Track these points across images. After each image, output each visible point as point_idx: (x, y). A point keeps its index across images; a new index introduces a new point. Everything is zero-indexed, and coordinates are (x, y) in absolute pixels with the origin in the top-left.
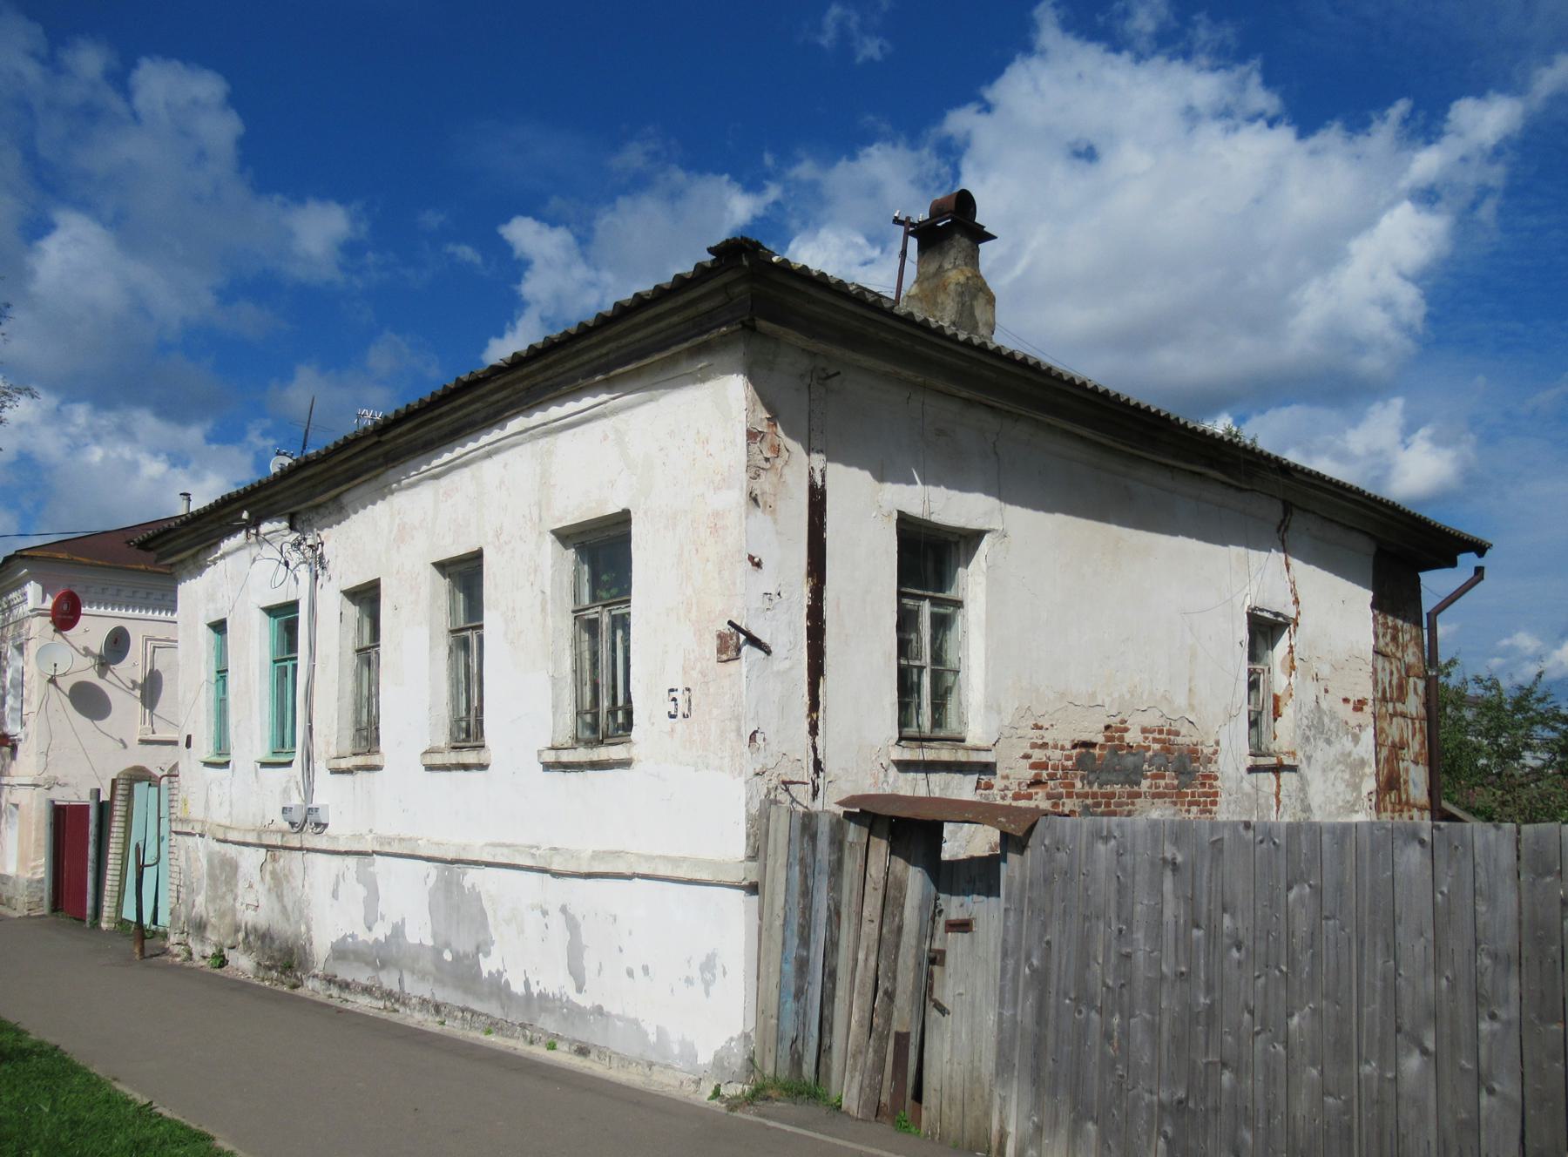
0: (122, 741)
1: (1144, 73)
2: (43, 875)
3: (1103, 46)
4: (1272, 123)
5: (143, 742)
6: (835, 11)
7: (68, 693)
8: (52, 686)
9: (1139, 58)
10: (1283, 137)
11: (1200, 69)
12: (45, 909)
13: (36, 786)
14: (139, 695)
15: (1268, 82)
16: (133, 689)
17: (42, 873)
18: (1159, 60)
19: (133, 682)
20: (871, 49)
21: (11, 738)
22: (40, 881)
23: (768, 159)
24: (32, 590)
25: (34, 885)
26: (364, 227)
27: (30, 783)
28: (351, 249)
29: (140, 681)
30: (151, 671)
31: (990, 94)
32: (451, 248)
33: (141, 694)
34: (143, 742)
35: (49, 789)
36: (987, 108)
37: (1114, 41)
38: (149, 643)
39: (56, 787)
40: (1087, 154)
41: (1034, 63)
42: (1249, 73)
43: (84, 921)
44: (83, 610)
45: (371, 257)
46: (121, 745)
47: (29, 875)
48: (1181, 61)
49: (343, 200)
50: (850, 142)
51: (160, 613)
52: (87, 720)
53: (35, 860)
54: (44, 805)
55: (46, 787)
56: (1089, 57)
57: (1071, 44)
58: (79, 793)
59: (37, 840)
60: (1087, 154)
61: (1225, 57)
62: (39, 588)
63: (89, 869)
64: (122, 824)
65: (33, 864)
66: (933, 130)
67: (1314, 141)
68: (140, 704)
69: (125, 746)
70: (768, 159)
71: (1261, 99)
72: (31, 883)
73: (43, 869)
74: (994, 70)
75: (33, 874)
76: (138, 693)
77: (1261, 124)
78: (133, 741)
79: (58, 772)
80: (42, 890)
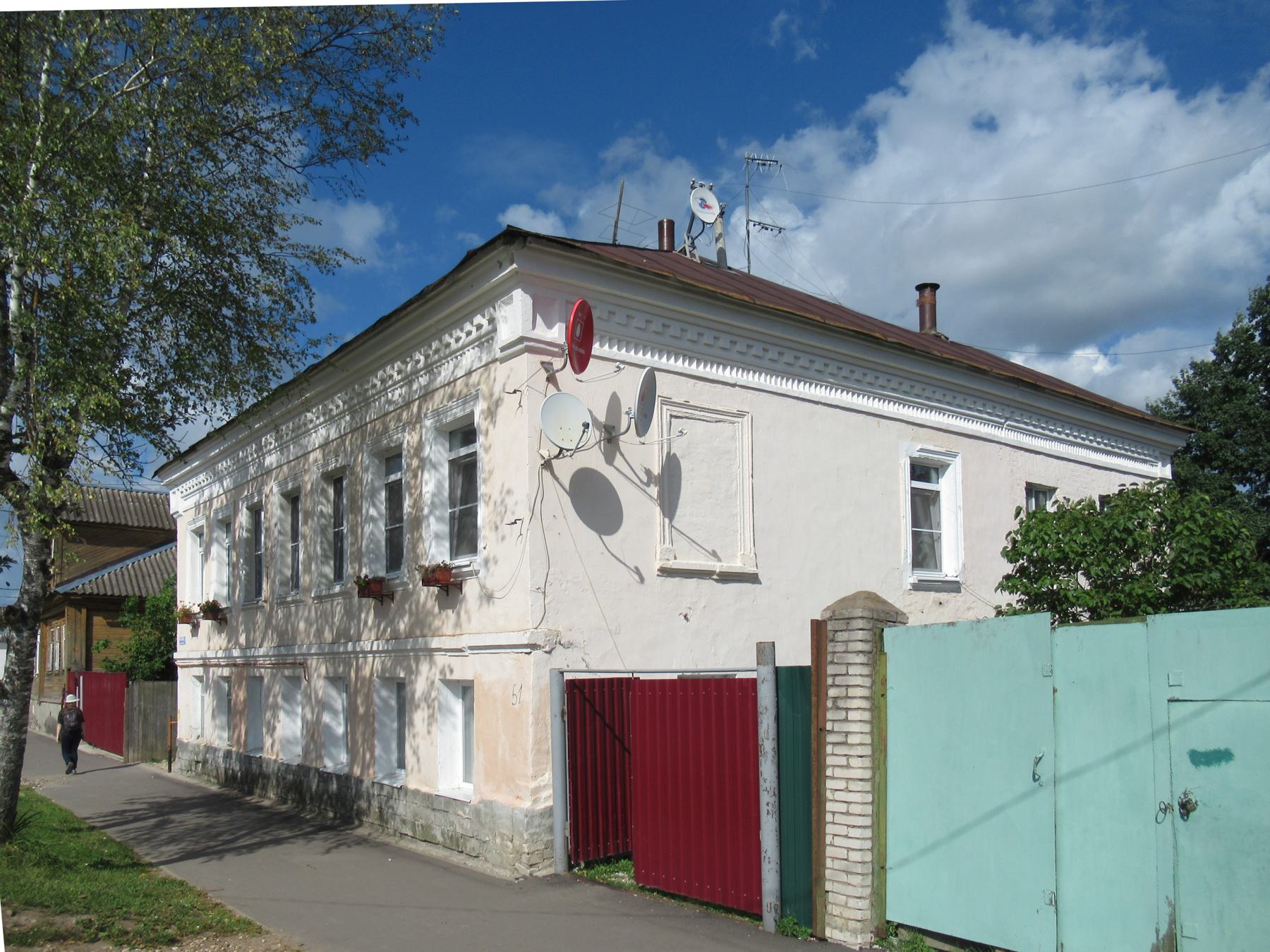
0: (637, 571)
1: (1042, 52)
2: (550, 803)
3: (1006, 31)
4: (1155, 87)
5: (666, 572)
6: (782, 17)
7: (567, 486)
8: (546, 474)
9: (1038, 38)
10: (1165, 97)
11: (1092, 46)
12: (556, 864)
13: (534, 647)
14: (655, 495)
15: (1153, 52)
16: (648, 484)
17: (547, 798)
18: (1058, 39)
19: (648, 472)
20: (806, 50)
21: (454, 571)
22: (549, 812)
23: (722, 143)
24: (518, 304)
25: (536, 822)
26: (394, 225)
27: (526, 642)
28: (384, 241)
29: (656, 470)
30: (668, 453)
31: (903, 82)
32: (460, 236)
33: (659, 492)
34: (666, 572)
35: (549, 652)
36: (904, 92)
37: (1016, 27)
38: (665, 407)
39: (559, 649)
40: (986, 124)
41: (943, 51)
42: (1135, 48)
43: (759, 917)
44: (596, 348)
45: (398, 246)
46: (637, 577)
47: (527, 804)
48: (1074, 41)
49: (378, 202)
50: (789, 127)
51: (676, 361)
52: (593, 535)
53: (535, 777)
54: (546, 680)
55: (547, 649)
56: (992, 41)
57: (979, 29)
58: (587, 659)
59: (537, 742)
60: (986, 124)
61: (1114, 32)
62: (529, 301)
63: (764, 809)
64: (866, 716)
65: (533, 785)
66: (858, 113)
67: (1193, 103)
68: (658, 509)
69: (642, 580)
70: (722, 143)
71: (1146, 65)
72: (532, 817)
73: (550, 792)
74: (909, 56)
75: (535, 801)
76: (654, 490)
77: (1146, 87)
78: (651, 570)
79: (557, 623)
80: (551, 829)
